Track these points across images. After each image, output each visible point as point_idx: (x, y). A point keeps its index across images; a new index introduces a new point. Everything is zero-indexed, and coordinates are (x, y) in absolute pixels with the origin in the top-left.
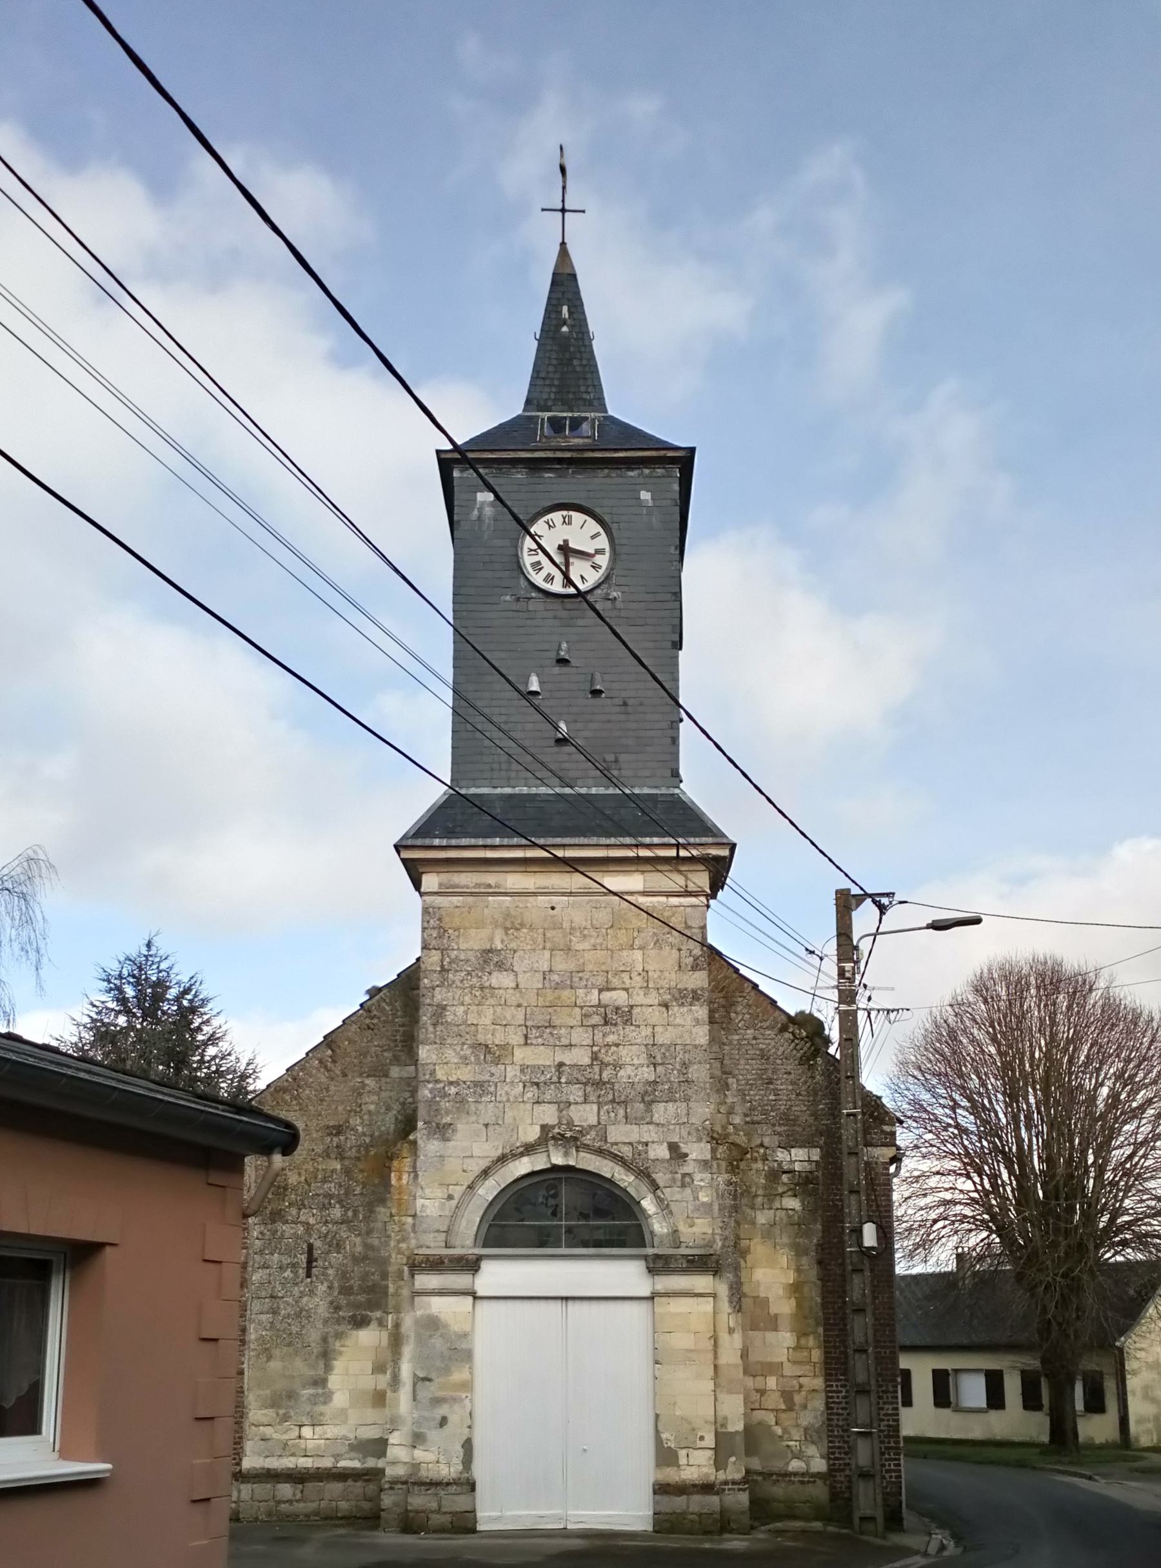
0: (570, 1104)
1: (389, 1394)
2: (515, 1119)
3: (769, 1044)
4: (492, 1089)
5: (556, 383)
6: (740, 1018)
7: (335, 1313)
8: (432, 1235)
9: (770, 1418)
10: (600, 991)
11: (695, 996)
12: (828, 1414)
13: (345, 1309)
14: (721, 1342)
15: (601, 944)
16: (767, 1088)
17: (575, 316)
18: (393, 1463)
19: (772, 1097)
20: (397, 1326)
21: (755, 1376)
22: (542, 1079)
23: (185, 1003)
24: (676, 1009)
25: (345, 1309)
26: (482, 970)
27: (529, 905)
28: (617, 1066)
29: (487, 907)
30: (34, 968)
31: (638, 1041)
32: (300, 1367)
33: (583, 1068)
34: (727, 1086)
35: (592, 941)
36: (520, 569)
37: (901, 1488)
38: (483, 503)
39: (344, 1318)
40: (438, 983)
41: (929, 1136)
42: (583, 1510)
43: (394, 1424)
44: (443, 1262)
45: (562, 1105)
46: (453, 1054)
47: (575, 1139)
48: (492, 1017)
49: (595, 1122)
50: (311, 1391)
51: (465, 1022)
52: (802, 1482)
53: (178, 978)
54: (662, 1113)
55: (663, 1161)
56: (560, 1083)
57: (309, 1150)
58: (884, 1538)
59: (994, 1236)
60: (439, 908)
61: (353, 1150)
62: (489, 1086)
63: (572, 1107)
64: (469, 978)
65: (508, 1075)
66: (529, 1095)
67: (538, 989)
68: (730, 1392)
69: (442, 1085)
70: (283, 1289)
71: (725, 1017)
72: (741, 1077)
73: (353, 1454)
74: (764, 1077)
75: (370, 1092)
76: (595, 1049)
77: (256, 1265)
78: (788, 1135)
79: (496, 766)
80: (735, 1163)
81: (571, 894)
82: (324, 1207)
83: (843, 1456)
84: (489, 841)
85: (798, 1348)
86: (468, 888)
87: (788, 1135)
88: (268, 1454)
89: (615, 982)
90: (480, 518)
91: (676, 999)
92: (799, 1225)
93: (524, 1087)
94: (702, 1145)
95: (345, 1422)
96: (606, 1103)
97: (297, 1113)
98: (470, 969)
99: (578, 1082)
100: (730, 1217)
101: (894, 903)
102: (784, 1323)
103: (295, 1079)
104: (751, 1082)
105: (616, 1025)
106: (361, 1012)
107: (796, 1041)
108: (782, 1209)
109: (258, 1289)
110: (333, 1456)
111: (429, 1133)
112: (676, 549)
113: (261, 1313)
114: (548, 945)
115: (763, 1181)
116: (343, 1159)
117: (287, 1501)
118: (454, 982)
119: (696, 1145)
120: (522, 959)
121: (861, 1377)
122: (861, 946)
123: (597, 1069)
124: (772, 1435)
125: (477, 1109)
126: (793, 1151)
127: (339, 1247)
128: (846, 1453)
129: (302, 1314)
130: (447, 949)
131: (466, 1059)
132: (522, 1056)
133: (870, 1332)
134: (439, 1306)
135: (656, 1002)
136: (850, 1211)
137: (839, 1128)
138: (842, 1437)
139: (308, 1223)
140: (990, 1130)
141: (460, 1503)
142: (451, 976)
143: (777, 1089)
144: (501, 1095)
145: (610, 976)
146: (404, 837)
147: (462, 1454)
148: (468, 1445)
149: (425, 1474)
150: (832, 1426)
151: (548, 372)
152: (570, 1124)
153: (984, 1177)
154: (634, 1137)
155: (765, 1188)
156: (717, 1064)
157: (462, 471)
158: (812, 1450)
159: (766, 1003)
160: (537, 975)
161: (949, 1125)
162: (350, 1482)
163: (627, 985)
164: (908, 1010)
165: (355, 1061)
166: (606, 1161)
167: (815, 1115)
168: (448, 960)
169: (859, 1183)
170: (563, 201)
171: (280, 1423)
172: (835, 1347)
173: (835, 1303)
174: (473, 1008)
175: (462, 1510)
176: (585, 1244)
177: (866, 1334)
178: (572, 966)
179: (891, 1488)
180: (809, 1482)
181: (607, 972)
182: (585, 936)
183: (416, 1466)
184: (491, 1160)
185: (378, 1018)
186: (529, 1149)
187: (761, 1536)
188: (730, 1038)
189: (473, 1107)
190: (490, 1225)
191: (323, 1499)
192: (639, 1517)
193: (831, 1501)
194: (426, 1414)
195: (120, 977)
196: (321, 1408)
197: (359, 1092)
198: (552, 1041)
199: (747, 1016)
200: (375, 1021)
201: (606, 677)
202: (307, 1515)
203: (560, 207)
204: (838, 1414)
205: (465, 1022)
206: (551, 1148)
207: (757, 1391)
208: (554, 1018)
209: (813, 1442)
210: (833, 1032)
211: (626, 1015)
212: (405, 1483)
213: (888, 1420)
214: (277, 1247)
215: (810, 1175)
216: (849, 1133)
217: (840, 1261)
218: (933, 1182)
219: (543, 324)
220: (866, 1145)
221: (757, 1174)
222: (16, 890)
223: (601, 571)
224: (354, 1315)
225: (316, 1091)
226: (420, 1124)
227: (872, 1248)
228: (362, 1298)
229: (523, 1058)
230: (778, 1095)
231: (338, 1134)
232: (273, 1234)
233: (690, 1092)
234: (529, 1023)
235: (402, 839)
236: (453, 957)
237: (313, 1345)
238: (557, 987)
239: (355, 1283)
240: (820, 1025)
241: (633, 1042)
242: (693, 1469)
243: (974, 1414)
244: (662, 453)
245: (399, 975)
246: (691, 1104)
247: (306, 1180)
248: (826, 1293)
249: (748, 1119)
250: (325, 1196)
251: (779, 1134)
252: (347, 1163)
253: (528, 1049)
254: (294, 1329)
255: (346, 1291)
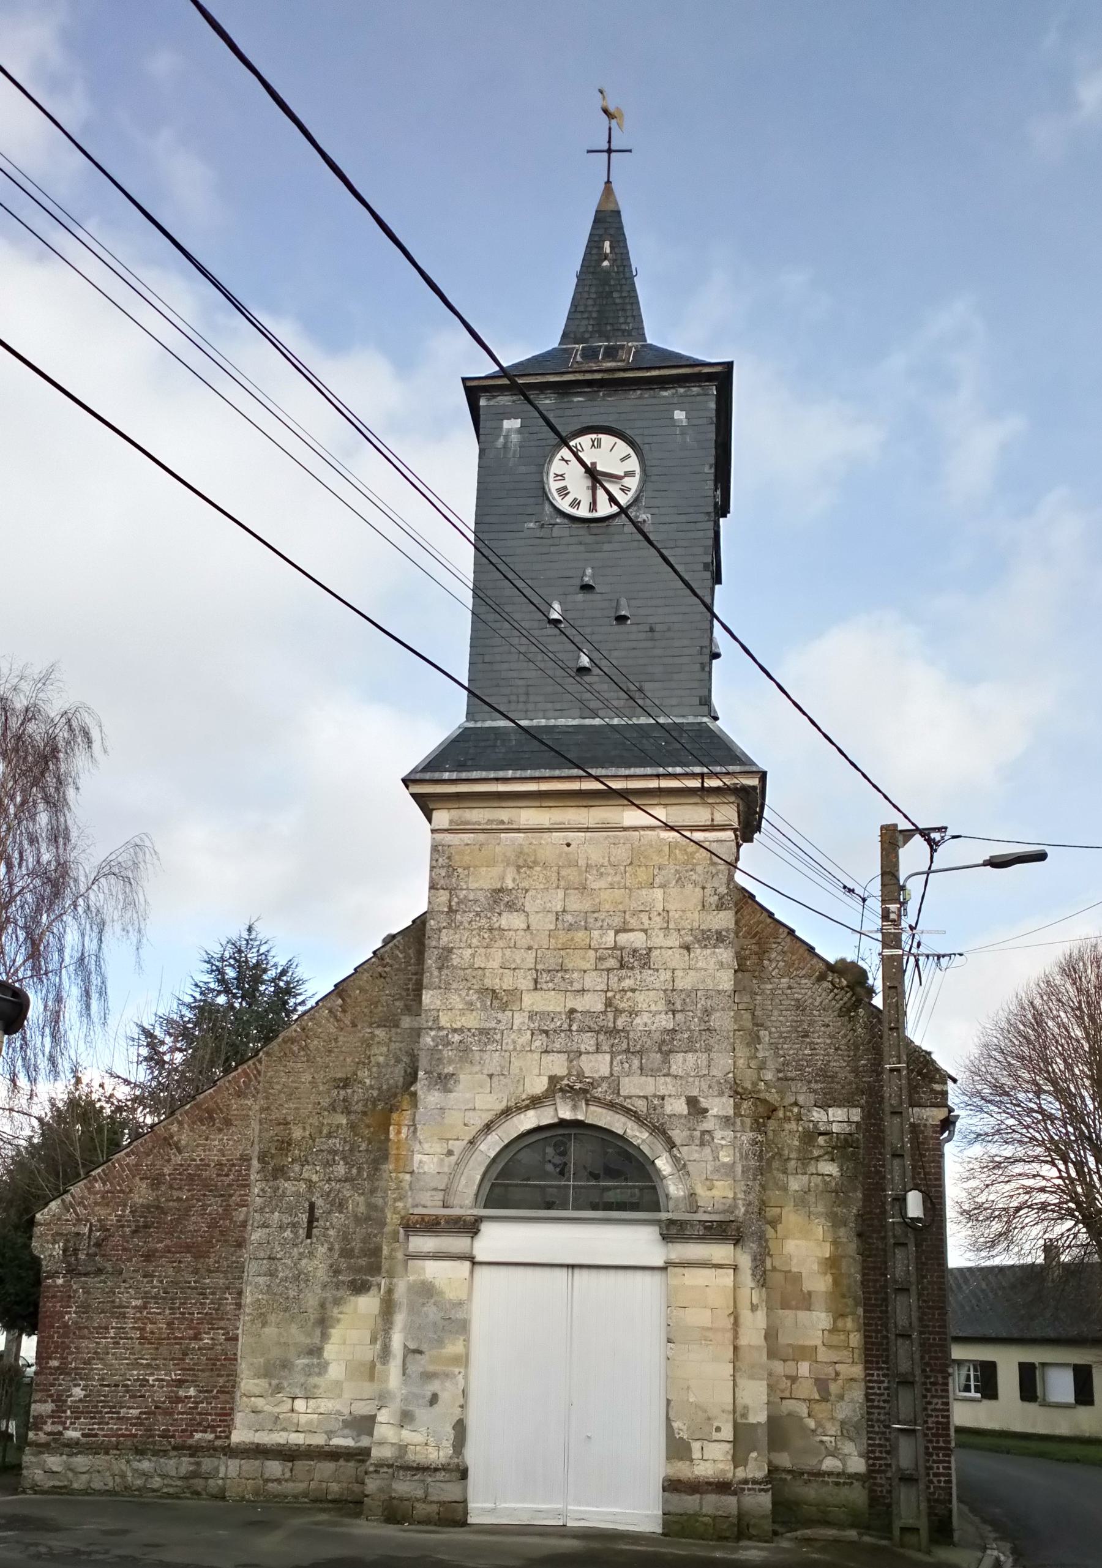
0: (581, 1054)
1: (378, 1366)
2: (521, 1069)
3: (806, 994)
4: (498, 1037)
5: (594, 315)
6: (774, 965)
7: (334, 1277)
8: (429, 1194)
9: (802, 1409)
10: (617, 932)
11: (720, 938)
12: (868, 1407)
13: (344, 1273)
14: (742, 1320)
15: (619, 883)
16: (803, 1042)
17: (617, 250)
18: (380, 1444)
19: (808, 1052)
20: (390, 1291)
21: (785, 1361)
22: (552, 1026)
23: (282, 984)
24: (698, 951)
25: (344, 1273)
26: (492, 910)
27: (543, 842)
28: (633, 1013)
29: (499, 844)
30: (135, 948)
31: (657, 986)
32: (297, 1335)
33: (595, 1015)
34: (758, 1039)
35: (610, 879)
36: (545, 495)
37: (951, 1494)
38: (509, 430)
39: (343, 1282)
40: (444, 924)
41: (1011, 1122)
42: (588, 1505)
43: (382, 1399)
44: (438, 1223)
45: (572, 1055)
46: (458, 1000)
47: (585, 1091)
48: (500, 960)
49: (607, 1074)
50: (306, 1361)
51: (471, 966)
52: (837, 1484)
53: (275, 960)
54: (680, 1064)
55: (680, 1116)
56: (570, 1030)
57: (315, 1103)
58: (929, 1553)
59: (1081, 1226)
60: (449, 846)
61: (360, 1104)
62: (495, 1034)
63: (583, 1057)
64: (478, 919)
65: (515, 1022)
66: (538, 1043)
67: (550, 931)
68: (752, 1377)
69: (445, 1032)
70: (282, 1250)
71: (758, 964)
72: (773, 1030)
73: (346, 1431)
74: (800, 1029)
75: (378, 1043)
76: (610, 994)
77: (256, 1224)
78: (825, 1094)
79: (514, 698)
80: (761, 1120)
81: (587, 829)
82: (327, 1164)
83: (884, 1455)
84: (501, 774)
85: (834, 1330)
86: (479, 825)
87: (825, 1094)
88: (258, 1427)
89: (633, 922)
90: (505, 446)
91: (699, 941)
92: (836, 1192)
93: (532, 1034)
94: (724, 1099)
95: (340, 1396)
96: (619, 1053)
97: (305, 1065)
98: (479, 909)
99: (591, 1030)
100: (755, 1179)
101: (946, 838)
102: (819, 1302)
103: (303, 1029)
104: (785, 1035)
105: (632, 968)
106: (373, 960)
107: (835, 991)
108: (818, 1174)
109: (257, 1249)
110: (326, 1433)
111: (430, 1083)
112: (711, 468)
113: (259, 1275)
114: (562, 883)
115: (797, 1143)
116: (349, 1113)
117: (276, 1480)
118: (461, 923)
119: (717, 1100)
120: (534, 898)
121: (904, 1366)
122: (908, 886)
123: (611, 1016)
124: (804, 1428)
125: (481, 1059)
126: (830, 1110)
127: (341, 1206)
128: (888, 1452)
129: (300, 1278)
130: (455, 889)
131: (472, 1005)
132: (530, 1002)
133: (915, 1315)
134: (434, 1271)
135: (677, 944)
136: (892, 1178)
137: (882, 1086)
138: (884, 1433)
139: (310, 1181)
140: (1074, 1115)
141: (449, 1491)
142: (458, 917)
143: (813, 1043)
144: (507, 1044)
145: (627, 917)
146: (413, 771)
147: (452, 1436)
148: (460, 1428)
149: (415, 1456)
150: (871, 1420)
151: (586, 306)
152: (581, 1075)
153: (1070, 1164)
154: (649, 1090)
155: (799, 1151)
156: (747, 1016)
157: (489, 400)
158: (849, 1448)
159: (802, 950)
160: (550, 915)
161: (1032, 1110)
162: (342, 1462)
163: (646, 926)
164: (961, 955)
165: (366, 1010)
166: (618, 1116)
167: (855, 1071)
168: (456, 900)
169: (903, 1147)
170: (609, 142)
171: (272, 1395)
172: (877, 1331)
173: (877, 1281)
174: (482, 951)
175: (449, 1500)
176: (594, 1207)
177: (910, 1317)
178: (587, 906)
179: (940, 1494)
180: (845, 1483)
181: (625, 912)
182: (602, 874)
183: (403, 1448)
184: (494, 1113)
185: (391, 966)
186: (535, 1102)
187: (785, 1544)
188: (762, 987)
189: (477, 1056)
190: (493, 1185)
191: (312, 1480)
192: (647, 1516)
193: (871, 1506)
194: (415, 1390)
195: (222, 959)
196: (315, 1380)
197: (368, 1044)
198: (563, 986)
199: (782, 964)
200: (387, 969)
201: (632, 602)
202: (295, 1497)
203: (606, 147)
204: (878, 1407)
205: (471, 966)
206: (558, 1101)
207: (788, 1377)
208: (566, 961)
209: (851, 1439)
210: (876, 980)
211: (643, 959)
212: (390, 1466)
213: (937, 1416)
214: (277, 1206)
215: (849, 1138)
216: (892, 1090)
217: (883, 1234)
218: (1018, 1168)
219: (584, 260)
220: (912, 1106)
221: (790, 1136)
222: (122, 874)
223: (631, 494)
224: (354, 1280)
225: (324, 1041)
226: (421, 1074)
227: (918, 1220)
228: (363, 1262)
229: (532, 1004)
230: (815, 1049)
231: (345, 1087)
232: (275, 1192)
233: (712, 1041)
234: (539, 967)
235: (411, 772)
236: (462, 897)
237: (310, 1310)
238: (570, 928)
239: (357, 1245)
240: (863, 974)
241: (650, 987)
242: (708, 1464)
243: (1059, 1410)
244: (696, 370)
245: (414, 922)
246: (713, 1055)
247: (310, 1135)
248: (865, 1271)
249: (781, 1075)
250: (329, 1152)
251: (815, 1091)
252: (353, 1117)
253: (538, 994)
254: (292, 1294)
255: (347, 1253)
